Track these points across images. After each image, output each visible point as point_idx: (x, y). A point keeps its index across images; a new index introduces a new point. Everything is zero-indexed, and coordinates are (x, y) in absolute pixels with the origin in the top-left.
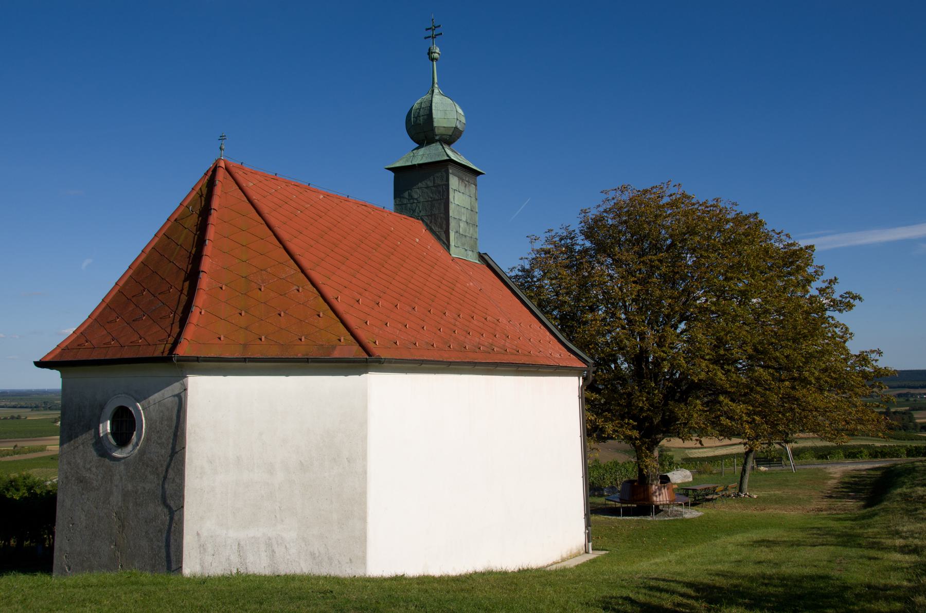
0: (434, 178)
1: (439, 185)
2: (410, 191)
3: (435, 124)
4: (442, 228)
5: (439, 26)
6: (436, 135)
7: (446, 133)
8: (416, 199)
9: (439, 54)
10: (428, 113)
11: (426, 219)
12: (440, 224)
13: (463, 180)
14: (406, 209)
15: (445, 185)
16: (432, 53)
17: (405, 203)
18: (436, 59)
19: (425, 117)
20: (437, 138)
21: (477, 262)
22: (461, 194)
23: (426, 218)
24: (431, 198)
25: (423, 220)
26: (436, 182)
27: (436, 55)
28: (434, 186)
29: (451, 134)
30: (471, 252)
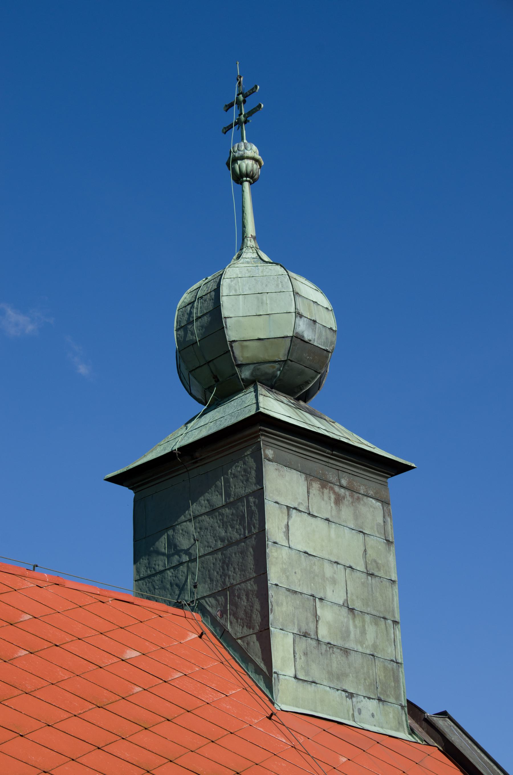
0: (227, 481)
1: (240, 499)
2: (170, 532)
3: (231, 334)
4: (250, 626)
5: (253, 91)
6: (240, 366)
7: (268, 358)
8: (187, 552)
9: (257, 161)
10: (211, 308)
11: (211, 605)
12: (246, 613)
13: (325, 483)
14: (164, 588)
15: (253, 494)
16: (235, 160)
17: (161, 568)
18: (252, 177)
19: (206, 319)
20: (246, 374)
21: (404, 735)
22: (323, 525)
23: (212, 600)
24: (222, 540)
25: (203, 611)
26: (233, 489)
27: (247, 165)
28: (227, 505)
29: (282, 357)
30: (375, 702)
